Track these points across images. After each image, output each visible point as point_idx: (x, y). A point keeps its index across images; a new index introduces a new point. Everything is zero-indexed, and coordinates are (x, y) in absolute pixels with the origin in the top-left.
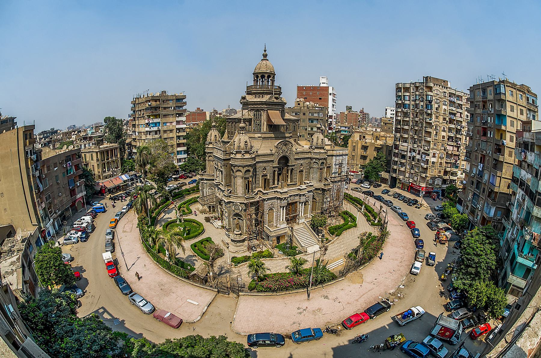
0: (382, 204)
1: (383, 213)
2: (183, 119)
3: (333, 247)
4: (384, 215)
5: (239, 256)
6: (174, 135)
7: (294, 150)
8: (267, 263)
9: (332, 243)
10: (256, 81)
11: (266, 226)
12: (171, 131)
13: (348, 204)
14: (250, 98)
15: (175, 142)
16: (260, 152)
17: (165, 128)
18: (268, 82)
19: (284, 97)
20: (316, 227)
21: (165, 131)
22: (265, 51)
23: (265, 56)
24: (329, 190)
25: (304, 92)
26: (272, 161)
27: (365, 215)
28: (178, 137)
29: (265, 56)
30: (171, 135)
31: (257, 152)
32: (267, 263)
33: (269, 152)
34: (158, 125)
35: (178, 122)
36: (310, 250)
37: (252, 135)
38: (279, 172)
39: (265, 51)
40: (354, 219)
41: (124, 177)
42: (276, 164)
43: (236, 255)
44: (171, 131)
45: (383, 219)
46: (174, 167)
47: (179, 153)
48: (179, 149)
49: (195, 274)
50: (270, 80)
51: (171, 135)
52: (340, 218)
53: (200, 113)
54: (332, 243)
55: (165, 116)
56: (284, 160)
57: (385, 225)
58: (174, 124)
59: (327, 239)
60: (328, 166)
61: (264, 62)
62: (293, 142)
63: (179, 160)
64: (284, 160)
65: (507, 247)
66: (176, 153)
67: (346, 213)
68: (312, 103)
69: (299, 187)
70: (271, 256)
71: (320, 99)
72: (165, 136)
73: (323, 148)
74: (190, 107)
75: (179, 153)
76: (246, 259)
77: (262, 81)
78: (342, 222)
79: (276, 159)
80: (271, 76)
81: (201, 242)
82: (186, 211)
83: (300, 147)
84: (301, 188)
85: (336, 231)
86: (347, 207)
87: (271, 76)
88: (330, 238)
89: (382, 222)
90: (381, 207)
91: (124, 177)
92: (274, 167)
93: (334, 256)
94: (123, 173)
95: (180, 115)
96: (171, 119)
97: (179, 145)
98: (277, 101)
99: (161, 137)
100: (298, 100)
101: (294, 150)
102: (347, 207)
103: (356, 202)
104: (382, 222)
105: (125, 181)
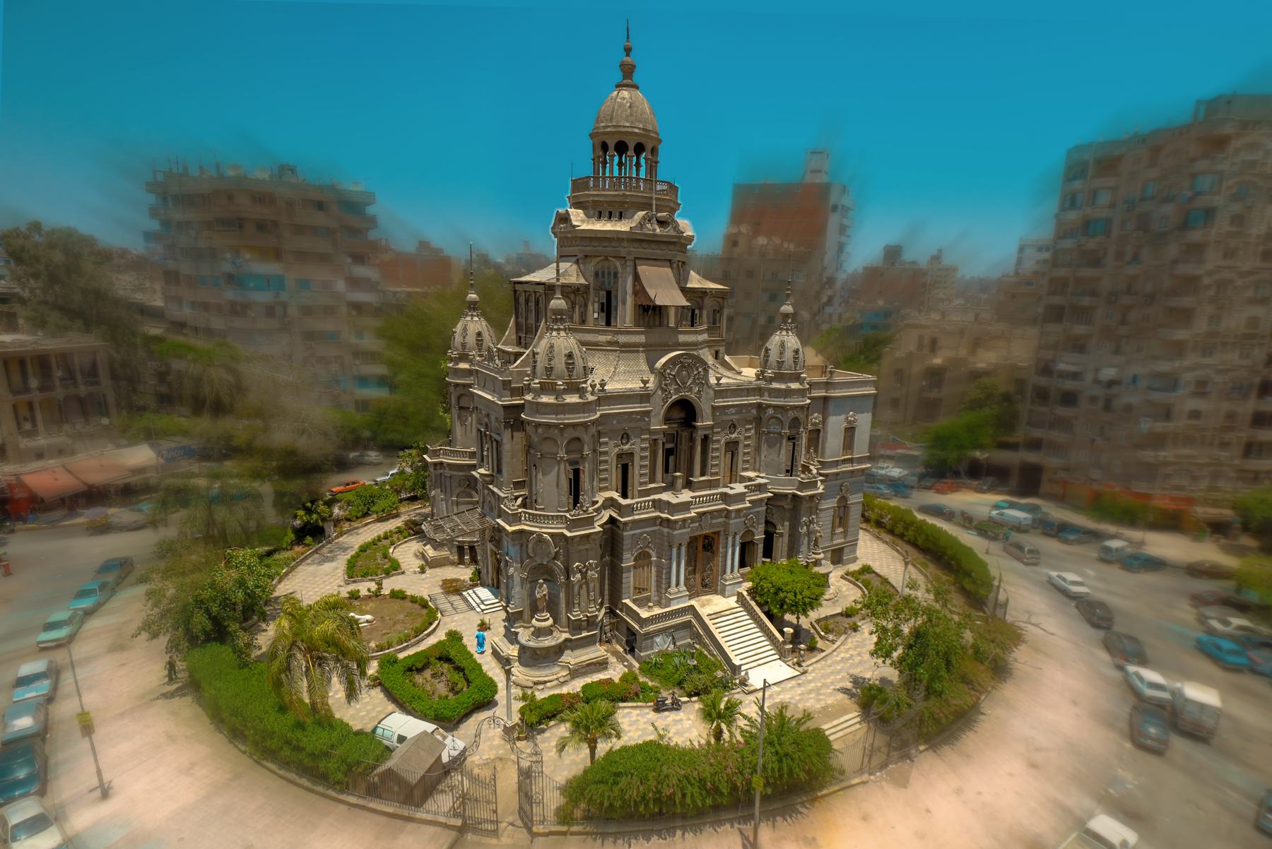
7: (713, 381)
18: (638, 165)
31: (603, 385)
39: (628, 50)
50: (643, 161)
56: (685, 412)
60: (810, 427)
62: (710, 360)
64: (685, 412)
73: (797, 378)
77: (620, 164)
79: (658, 408)
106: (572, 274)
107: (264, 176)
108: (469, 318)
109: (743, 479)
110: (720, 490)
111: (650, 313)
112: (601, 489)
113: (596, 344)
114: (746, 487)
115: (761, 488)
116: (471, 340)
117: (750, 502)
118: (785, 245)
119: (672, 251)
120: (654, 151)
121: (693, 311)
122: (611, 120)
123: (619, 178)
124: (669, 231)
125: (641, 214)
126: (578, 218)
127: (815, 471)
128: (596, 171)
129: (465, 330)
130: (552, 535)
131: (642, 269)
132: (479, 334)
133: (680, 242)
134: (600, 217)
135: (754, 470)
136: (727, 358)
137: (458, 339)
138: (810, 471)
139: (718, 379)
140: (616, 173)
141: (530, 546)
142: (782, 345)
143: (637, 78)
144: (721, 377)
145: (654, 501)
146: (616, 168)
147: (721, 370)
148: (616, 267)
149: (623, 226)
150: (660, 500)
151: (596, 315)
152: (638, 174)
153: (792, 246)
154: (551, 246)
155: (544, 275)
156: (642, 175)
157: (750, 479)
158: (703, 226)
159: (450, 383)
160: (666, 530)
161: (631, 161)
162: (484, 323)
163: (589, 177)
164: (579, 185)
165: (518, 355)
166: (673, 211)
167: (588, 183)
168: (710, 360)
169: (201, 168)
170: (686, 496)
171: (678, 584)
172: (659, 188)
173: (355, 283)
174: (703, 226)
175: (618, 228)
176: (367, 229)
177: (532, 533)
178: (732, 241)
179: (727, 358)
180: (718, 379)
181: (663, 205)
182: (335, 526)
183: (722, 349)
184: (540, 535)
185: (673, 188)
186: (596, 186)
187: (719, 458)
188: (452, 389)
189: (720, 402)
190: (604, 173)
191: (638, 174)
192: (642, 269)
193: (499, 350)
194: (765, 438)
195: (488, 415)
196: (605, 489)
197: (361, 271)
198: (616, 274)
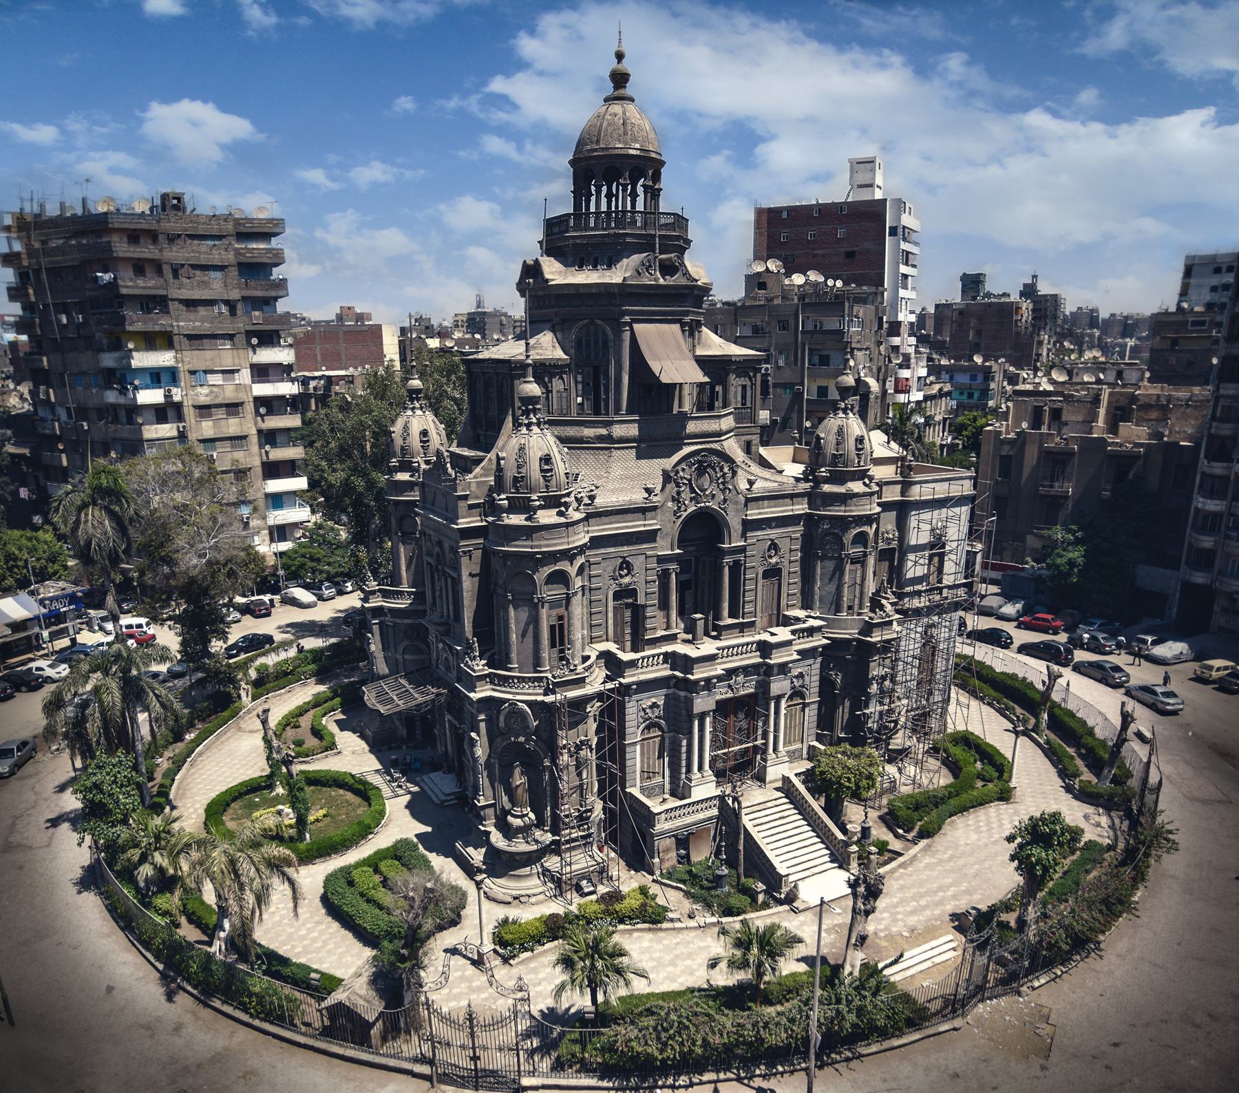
0: (1131, 705)
2: (282, 355)
4: (1142, 751)
5: (527, 915)
7: (743, 485)
8: (637, 945)
11: (635, 791)
12: (233, 408)
13: (974, 704)
14: (555, 273)
15: (252, 457)
16: (602, 501)
17: (203, 395)
18: (634, 195)
20: (827, 792)
21: (204, 410)
22: (620, 56)
23: (620, 79)
25: (784, 231)
26: (651, 536)
27: (1050, 753)
28: (269, 437)
29: (620, 79)
30: (233, 426)
31: (592, 498)
32: (637, 945)
33: (638, 497)
35: (262, 372)
36: (809, 894)
37: (571, 431)
38: (684, 577)
39: (620, 56)
40: (998, 767)
42: (664, 548)
43: (513, 913)
44: (233, 408)
45: (1137, 770)
46: (257, 559)
47: (277, 500)
50: (640, 190)
51: (233, 426)
52: (933, 763)
55: (195, 339)
56: (703, 531)
57: (1149, 798)
58: (245, 376)
59: (882, 847)
60: (882, 546)
61: (616, 108)
62: (739, 455)
63: (280, 533)
64: (703, 531)
65: (220, 413)
67: (967, 740)
69: (765, 637)
70: (652, 916)
72: (207, 428)
73: (862, 475)
75: (277, 500)
76: (553, 928)
77: (609, 196)
78: (944, 779)
79: (666, 524)
80: (646, 168)
81: (373, 863)
83: (766, 473)
84: (773, 640)
85: (918, 818)
86: (971, 716)
87: (646, 168)
88: (896, 845)
89: (1134, 783)
90: (1127, 718)
92: (661, 560)
93: (912, 920)
95: (269, 339)
96: (226, 355)
97: (273, 470)
99: (182, 436)
100: (759, 268)
101: (743, 485)
102: (971, 716)
103: (1006, 693)
104: (1134, 783)
106: (547, 347)
107: (141, 207)
108: (409, 413)
109: (786, 621)
110: (757, 638)
111: (652, 397)
112: (592, 640)
113: (580, 440)
114: (793, 632)
115: (811, 631)
116: (415, 441)
117: (799, 652)
118: (830, 282)
119: (684, 303)
120: (657, 177)
121: (712, 389)
122: (598, 142)
123: (608, 213)
124: (676, 280)
125: (636, 258)
126: (555, 273)
127: (889, 608)
128: (577, 206)
129: (406, 427)
130: (530, 704)
131: (636, 326)
132: (424, 433)
133: (696, 294)
134: (581, 267)
135: (804, 607)
136: (762, 451)
137: (398, 442)
138: (882, 607)
139: (751, 483)
140: (604, 208)
141: (502, 718)
142: (840, 432)
143: (629, 90)
144: (751, 478)
145: (666, 655)
146: (604, 200)
147: (755, 469)
148: (605, 334)
149: (615, 276)
150: (674, 653)
151: (579, 400)
152: (633, 206)
153: (839, 284)
154: (517, 308)
155: (511, 349)
156: (640, 206)
157: (797, 620)
158: (721, 260)
159: (389, 501)
160: (682, 694)
161: (625, 190)
162: (430, 416)
163: (568, 215)
164: (554, 227)
165: (478, 461)
166: (681, 251)
167: (568, 221)
168: (739, 455)
169: (62, 205)
170: (708, 647)
171: (700, 768)
172: (663, 221)
173: (262, 372)
174: (721, 260)
175: (607, 280)
176: (276, 299)
177: (505, 701)
178: (756, 282)
179: (762, 451)
180: (751, 483)
181: (671, 240)
182: (237, 479)
183: (756, 439)
184: (513, 704)
185: (680, 221)
186: (577, 227)
187: (756, 592)
188: (391, 508)
189: (754, 514)
190: (588, 207)
191: (633, 206)
192: (636, 326)
193: (452, 454)
194: (859, 696)
195: (440, 543)
196: (598, 639)
197: (267, 356)
198: (605, 343)
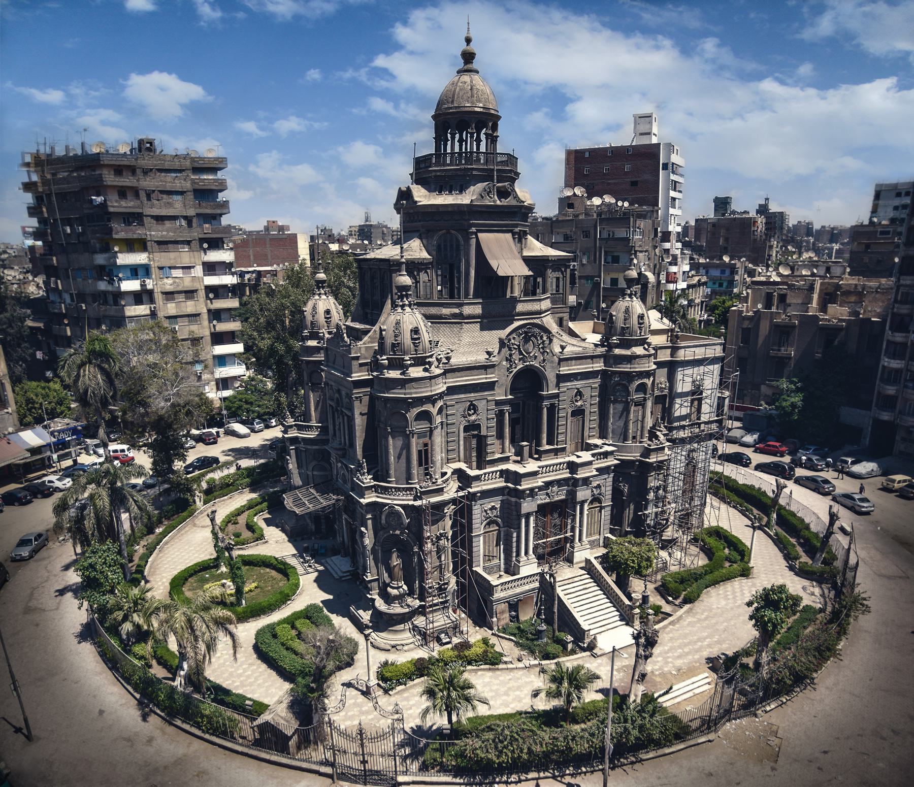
0: (836, 508)
1: (839, 536)
2: (225, 256)
3: (676, 634)
4: (844, 541)
5: (402, 658)
6: (199, 305)
7: (557, 350)
8: (481, 680)
9: (671, 623)
10: (440, 138)
11: (479, 570)
12: (190, 294)
15: (203, 329)
17: (168, 284)
18: (479, 141)
19: (524, 192)
20: (617, 570)
21: (169, 295)
22: (468, 41)
23: (468, 57)
24: (660, 465)
25: (586, 167)
26: (490, 386)
27: (778, 542)
28: (216, 315)
29: (468, 57)
30: (190, 307)
31: (448, 358)
32: (481, 680)
33: (482, 358)
34: (140, 272)
35: (211, 268)
36: (604, 643)
39: (468, 41)
41: (32, 438)
42: (500, 394)
43: (391, 657)
44: (190, 294)
45: (840, 555)
46: (207, 402)
47: (222, 360)
48: (220, 350)
49: (267, 723)
50: (483, 137)
51: (190, 307)
52: (694, 550)
53: (278, 241)
54: (671, 623)
55: (163, 244)
56: (528, 383)
57: (849, 575)
58: (198, 271)
60: (657, 393)
61: (466, 78)
62: (554, 328)
63: (224, 383)
64: (528, 383)
66: (210, 362)
67: (718, 533)
68: (609, 199)
69: (573, 458)
70: (491, 660)
71: (634, 183)
72: (171, 308)
73: (643, 342)
74: (245, 213)
75: (222, 360)
76: (420, 668)
78: (702, 561)
79: (501, 377)
80: (487, 121)
81: (291, 621)
82: (246, 534)
84: (578, 461)
85: (683, 589)
87: (487, 121)
88: (667, 608)
89: (838, 564)
90: (833, 517)
91: (32, 438)
92: (498, 403)
93: (679, 663)
94: (24, 425)
95: (216, 244)
96: (185, 256)
97: (219, 338)
98: (505, 202)
99: (153, 314)
100: (569, 193)
101: (557, 350)
104: (838, 564)
105: (34, 451)
